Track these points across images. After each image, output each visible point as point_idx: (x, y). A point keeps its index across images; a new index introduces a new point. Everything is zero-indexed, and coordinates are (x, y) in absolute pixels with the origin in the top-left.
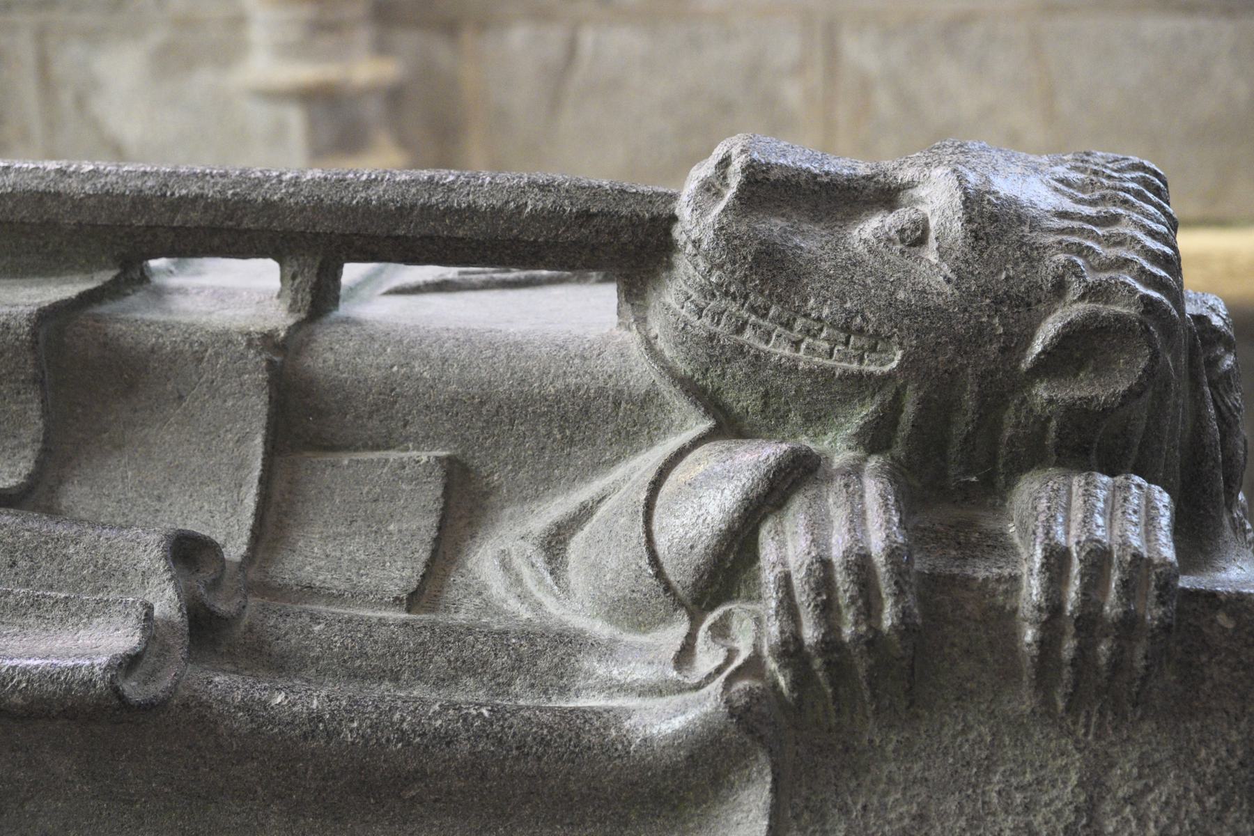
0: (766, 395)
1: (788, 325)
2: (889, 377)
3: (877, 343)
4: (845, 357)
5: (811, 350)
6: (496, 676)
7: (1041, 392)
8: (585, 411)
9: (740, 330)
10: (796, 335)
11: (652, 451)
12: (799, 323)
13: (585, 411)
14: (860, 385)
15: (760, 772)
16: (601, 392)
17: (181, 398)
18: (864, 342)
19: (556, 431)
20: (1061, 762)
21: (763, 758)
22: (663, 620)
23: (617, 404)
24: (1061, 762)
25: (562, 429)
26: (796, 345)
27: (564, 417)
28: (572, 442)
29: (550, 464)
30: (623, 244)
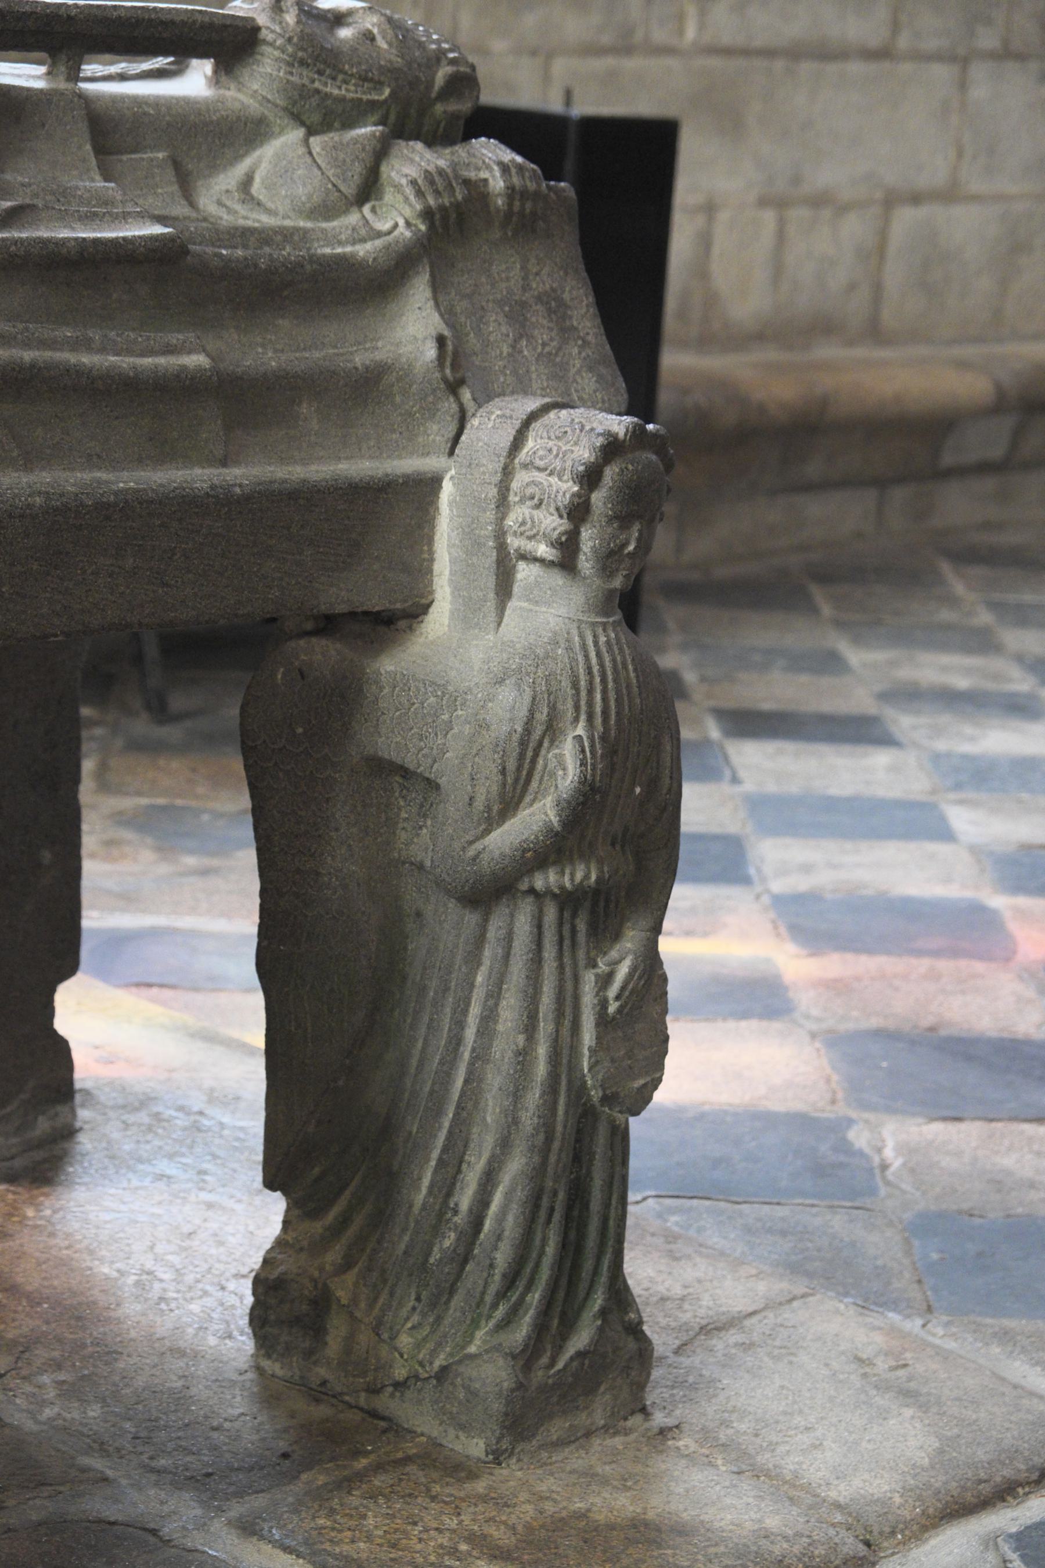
0: (325, 115)
1: (334, 79)
2: (386, 101)
3: (378, 85)
4: (364, 93)
5: (347, 90)
6: (278, 245)
7: (439, 108)
8: (231, 129)
9: (313, 81)
10: (338, 83)
11: (482, 86)
12: (340, 77)
13: (231, 129)
14: (373, 105)
15: (423, 267)
16: (239, 118)
17: (43, 125)
18: (371, 85)
19: (217, 141)
20: (513, 260)
21: (425, 260)
22: (344, 212)
23: (246, 124)
24: (513, 260)
25: (220, 139)
26: (340, 88)
27: (221, 133)
28: (224, 145)
29: (214, 157)
30: (230, 45)
